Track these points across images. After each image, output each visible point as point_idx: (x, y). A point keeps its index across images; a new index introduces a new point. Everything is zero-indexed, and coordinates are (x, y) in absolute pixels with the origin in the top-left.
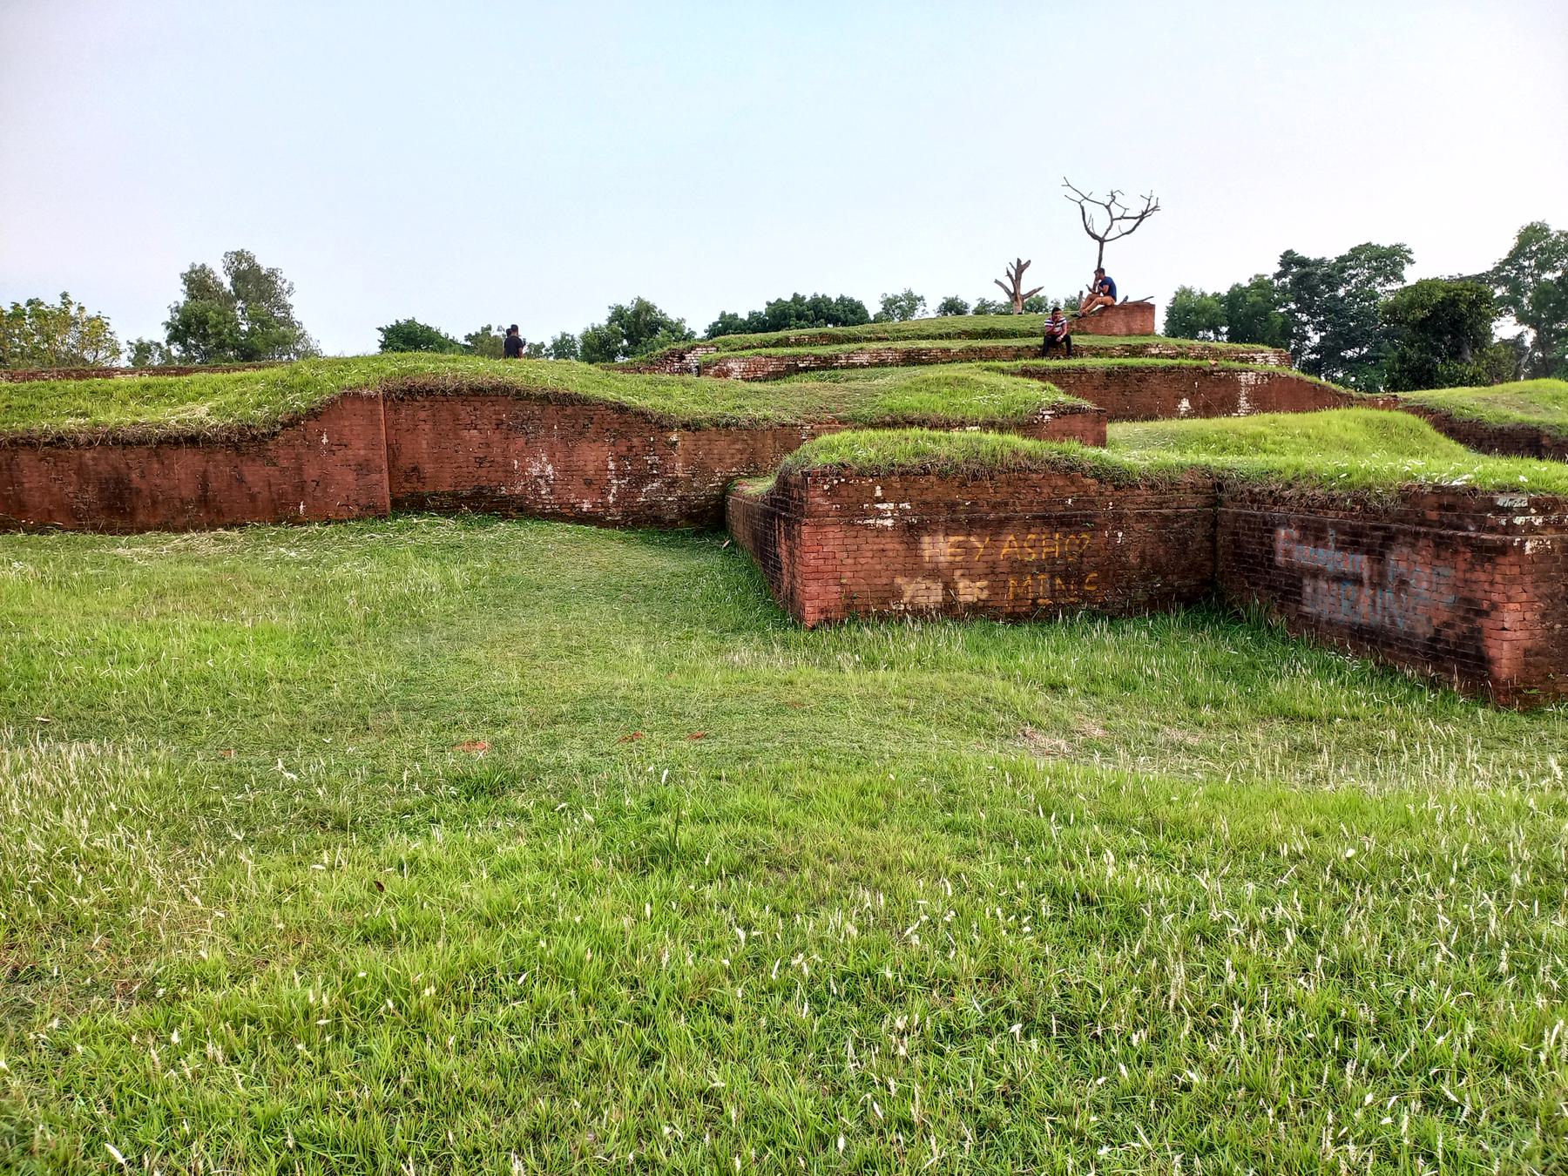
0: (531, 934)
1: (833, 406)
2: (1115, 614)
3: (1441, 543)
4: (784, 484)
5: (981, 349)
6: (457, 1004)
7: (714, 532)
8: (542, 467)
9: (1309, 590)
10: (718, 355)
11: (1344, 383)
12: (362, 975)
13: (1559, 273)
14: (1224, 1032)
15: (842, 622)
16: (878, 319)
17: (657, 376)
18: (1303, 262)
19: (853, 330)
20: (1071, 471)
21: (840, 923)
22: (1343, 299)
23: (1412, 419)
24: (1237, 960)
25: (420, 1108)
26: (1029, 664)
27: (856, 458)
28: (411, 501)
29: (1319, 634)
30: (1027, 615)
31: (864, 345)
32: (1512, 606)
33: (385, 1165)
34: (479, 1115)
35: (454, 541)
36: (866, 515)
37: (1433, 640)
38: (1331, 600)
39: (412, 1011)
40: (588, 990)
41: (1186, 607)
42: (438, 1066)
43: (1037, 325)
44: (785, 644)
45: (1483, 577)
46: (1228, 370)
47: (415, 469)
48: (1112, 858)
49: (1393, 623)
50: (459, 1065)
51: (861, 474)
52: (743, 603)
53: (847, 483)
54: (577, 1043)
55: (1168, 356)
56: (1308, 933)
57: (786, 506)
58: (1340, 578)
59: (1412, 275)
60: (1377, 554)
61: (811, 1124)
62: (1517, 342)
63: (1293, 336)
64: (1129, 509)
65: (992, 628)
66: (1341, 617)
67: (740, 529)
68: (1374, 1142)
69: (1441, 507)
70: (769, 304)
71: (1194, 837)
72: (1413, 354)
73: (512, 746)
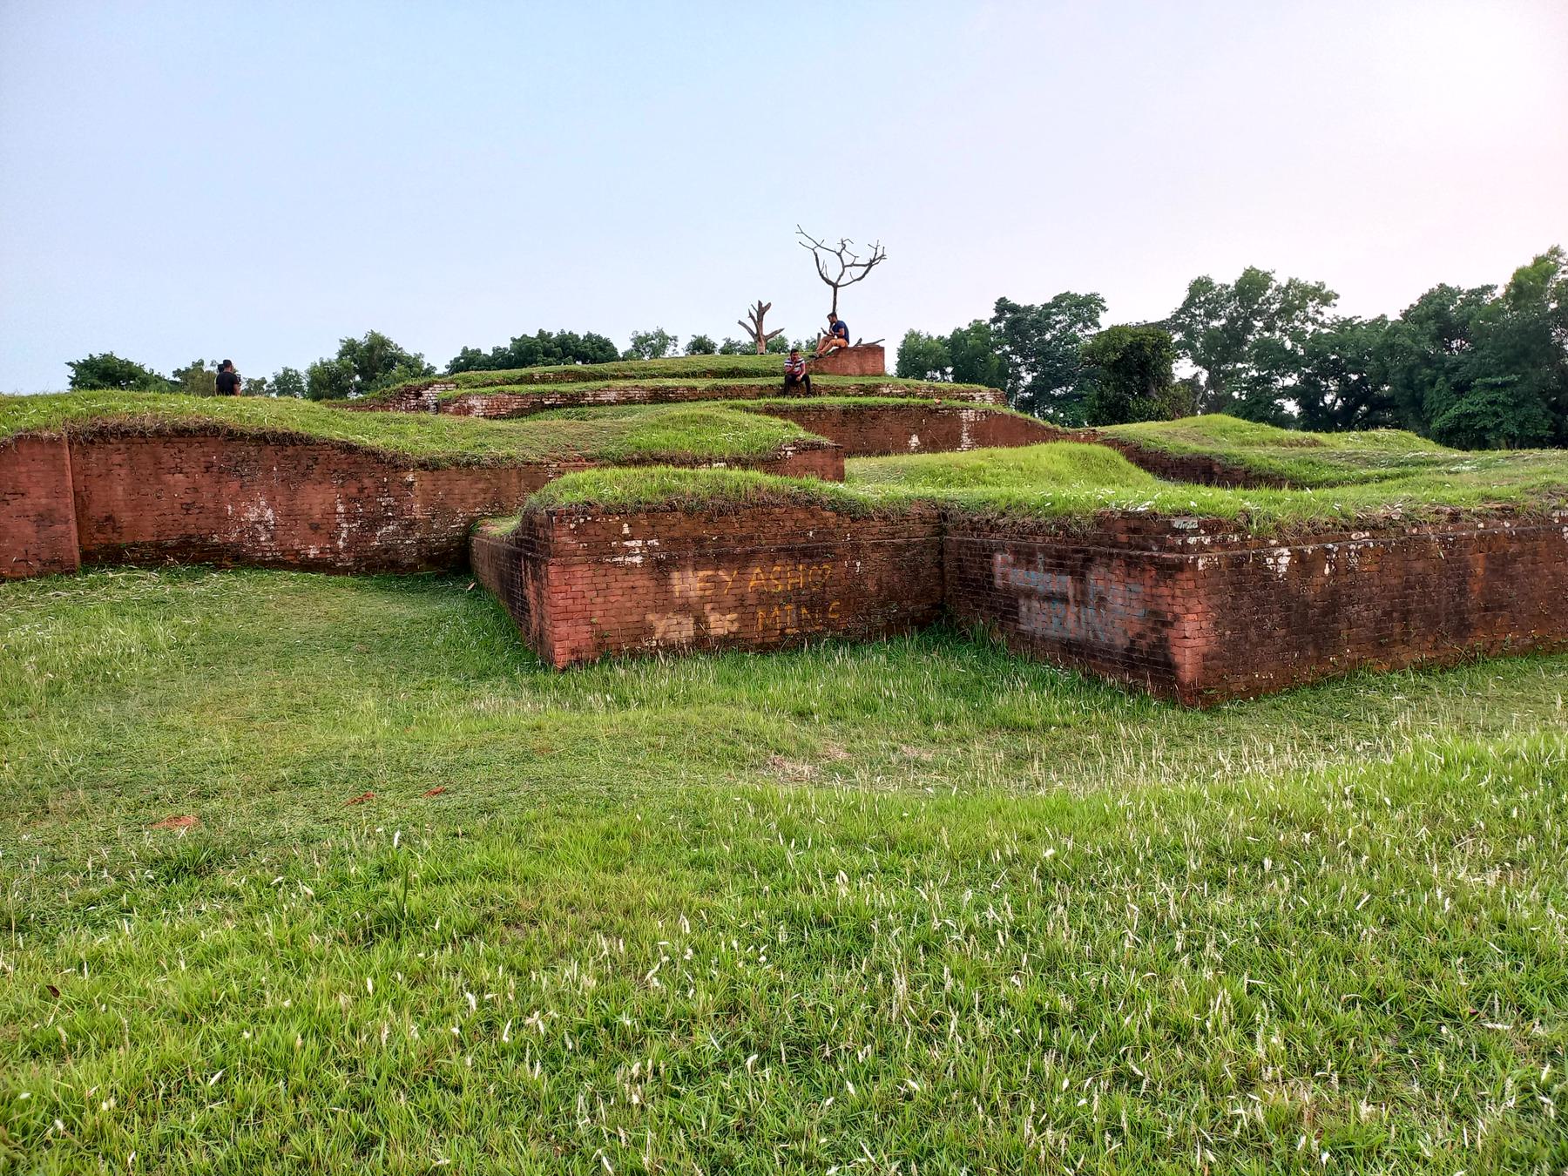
1: (579, 443)
2: (855, 641)
3: (1131, 563)
4: (529, 523)
5: (726, 388)
6: (142, 1115)
7: (457, 574)
8: (260, 512)
9: (1024, 609)
10: (459, 392)
11: (1052, 419)
12: (24, 1096)
13: (1223, 321)
15: (593, 662)
16: (628, 356)
18: (1014, 309)
19: (598, 367)
20: (811, 504)
24: (956, 966)
27: (602, 496)
28: (105, 552)
29: (1030, 648)
30: (777, 646)
31: (611, 382)
32: (1191, 617)
35: (158, 595)
36: (614, 553)
37: (1130, 650)
38: (1044, 618)
39: (86, 1130)
40: (299, 1079)
41: (920, 630)
44: (534, 687)
45: (1166, 592)
46: (950, 408)
47: (108, 519)
49: (1096, 636)
51: (607, 512)
52: (489, 648)
53: (593, 521)
54: (284, 1139)
55: (898, 395)
57: (531, 547)
58: (1049, 598)
59: (1106, 321)
60: (1080, 576)
62: (1192, 383)
63: (1009, 376)
64: (866, 540)
67: (486, 572)
70: (514, 340)
71: (923, 849)
72: (1109, 392)
73: (223, 819)
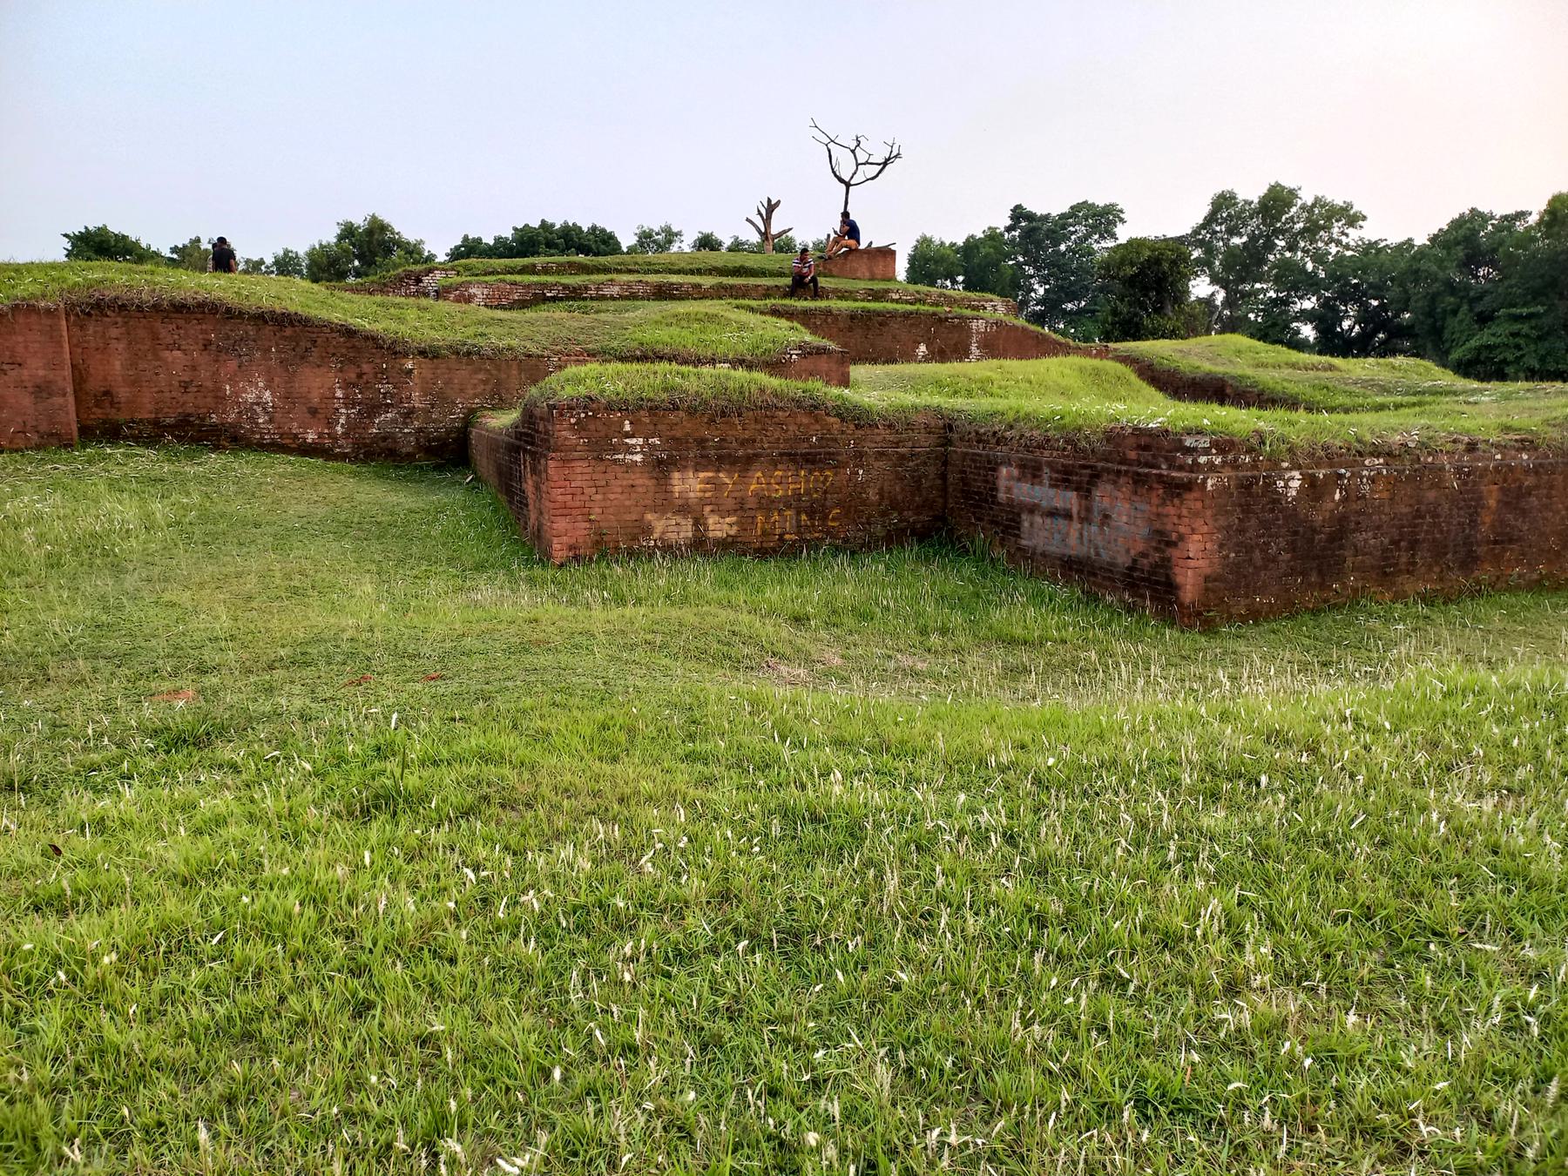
0: (235, 891)
1: (581, 338)
2: (855, 549)
3: (1139, 480)
4: (529, 417)
5: (732, 287)
6: (144, 970)
8: (257, 393)
9: (1026, 524)
10: (459, 279)
11: (1064, 333)
12: (28, 946)
13: (1245, 239)
14: (932, 931)
15: (591, 559)
16: (631, 250)
17: (392, 298)
18: (1030, 217)
20: (815, 408)
21: (575, 859)
22: (1064, 254)
23: (1120, 367)
25: (94, 1085)
26: (773, 598)
27: (603, 391)
28: (102, 426)
30: (775, 551)
31: (614, 276)
32: (1196, 537)
33: (49, 1150)
34: (165, 1085)
35: (156, 473)
36: (616, 450)
37: (1131, 569)
38: (1046, 534)
40: (298, 943)
41: (920, 541)
42: (117, 1038)
43: (786, 265)
44: (531, 581)
46: (960, 317)
48: (839, 776)
49: (1098, 554)
50: (143, 1035)
51: (609, 408)
52: (487, 541)
54: (282, 999)
55: (907, 302)
56: (1012, 837)
57: (530, 440)
58: (1053, 513)
59: (1124, 234)
60: (1085, 490)
61: (533, 1058)
62: (1208, 302)
63: (1020, 288)
65: (740, 563)
66: (1053, 549)
67: (484, 463)
68: (1058, 1021)
69: (1139, 447)
70: (515, 229)
71: (916, 753)
73: (221, 694)
